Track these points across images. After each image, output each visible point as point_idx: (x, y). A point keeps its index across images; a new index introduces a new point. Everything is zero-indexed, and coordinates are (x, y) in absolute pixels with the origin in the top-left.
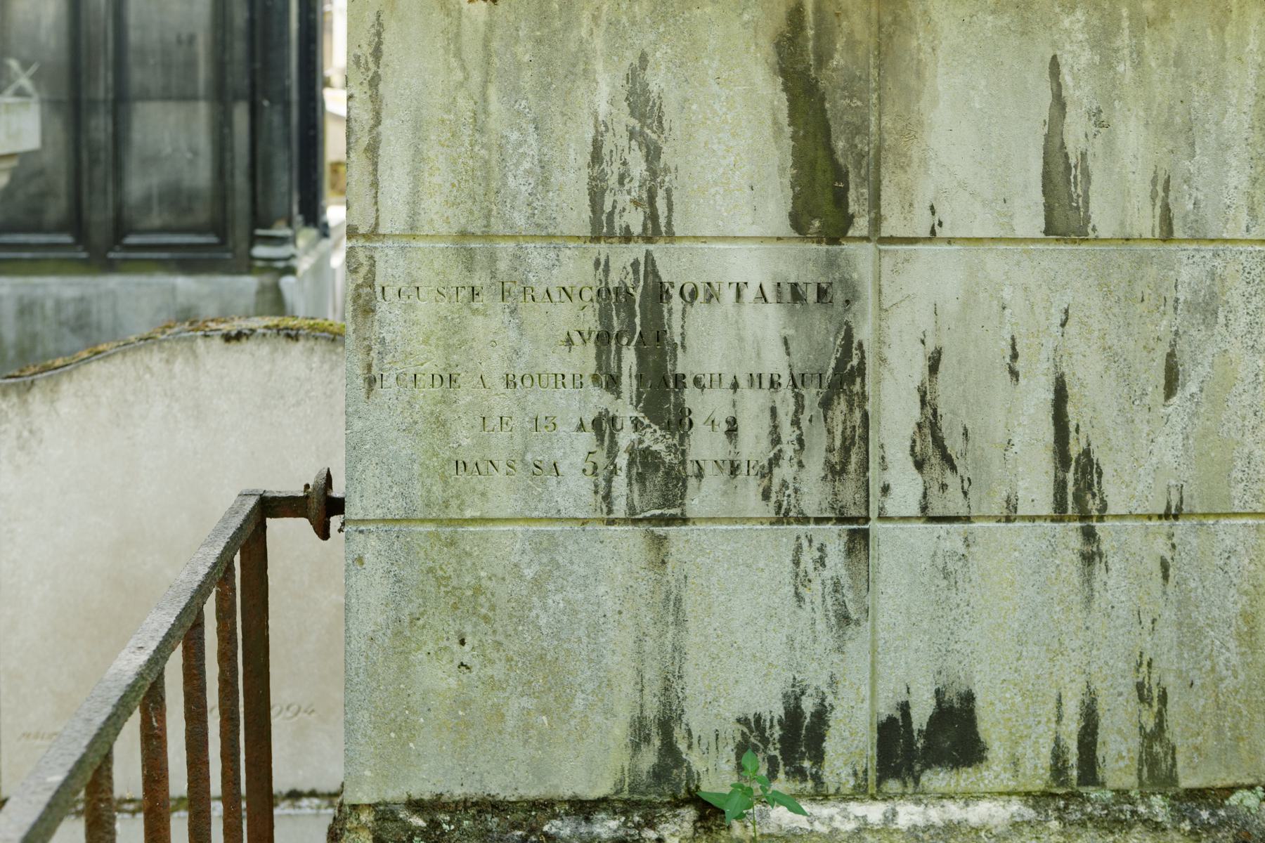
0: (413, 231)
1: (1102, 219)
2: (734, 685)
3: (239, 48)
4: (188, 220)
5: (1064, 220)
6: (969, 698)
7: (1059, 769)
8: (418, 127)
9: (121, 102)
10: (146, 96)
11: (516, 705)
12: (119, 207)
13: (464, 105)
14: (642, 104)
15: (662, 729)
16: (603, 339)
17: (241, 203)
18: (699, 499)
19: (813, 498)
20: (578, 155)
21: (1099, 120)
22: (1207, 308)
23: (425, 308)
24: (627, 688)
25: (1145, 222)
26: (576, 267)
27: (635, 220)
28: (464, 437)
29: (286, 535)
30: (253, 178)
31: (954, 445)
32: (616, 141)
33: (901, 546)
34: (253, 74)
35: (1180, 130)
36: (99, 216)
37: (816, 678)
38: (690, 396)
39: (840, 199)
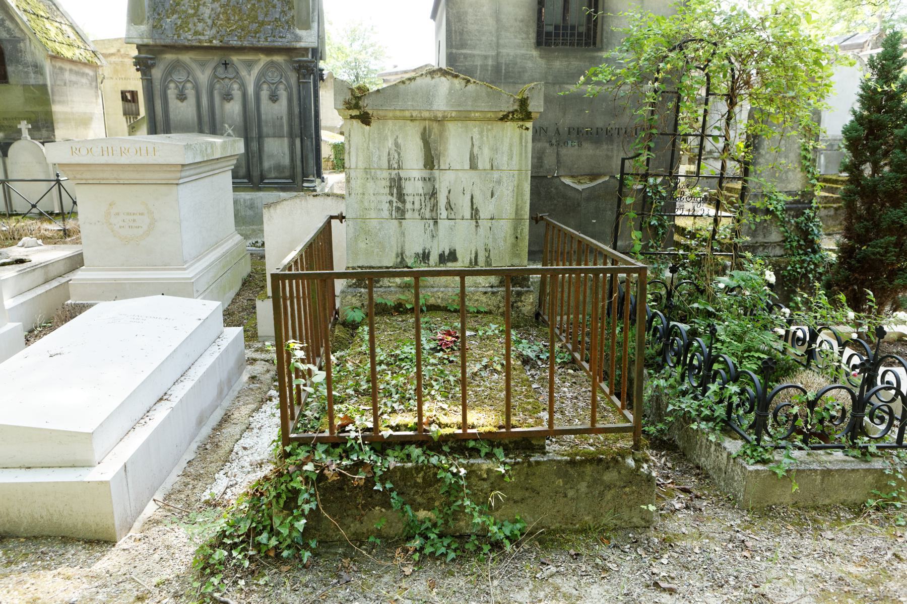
0: (356, 168)
1: (480, 166)
2: (414, 247)
3: (297, 121)
4: (283, 175)
5: (473, 166)
6: (455, 250)
7: (471, 263)
8: (357, 149)
9: (260, 138)
10: (268, 136)
11: (376, 250)
12: (261, 171)
13: (365, 145)
14: (397, 145)
15: (401, 255)
16: (390, 187)
17: (299, 170)
18: (407, 216)
19: (428, 215)
20: (386, 154)
21: (480, 148)
22: (499, 182)
23: (359, 181)
24: (395, 247)
25: (488, 167)
26: (385, 174)
27: (396, 166)
28: (366, 204)
29: (335, 223)
30: (302, 162)
31: (453, 206)
32: (392, 152)
33: (443, 224)
34: (301, 129)
35: (495, 150)
36: (256, 174)
37: (428, 246)
38: (406, 197)
39: (433, 162)
